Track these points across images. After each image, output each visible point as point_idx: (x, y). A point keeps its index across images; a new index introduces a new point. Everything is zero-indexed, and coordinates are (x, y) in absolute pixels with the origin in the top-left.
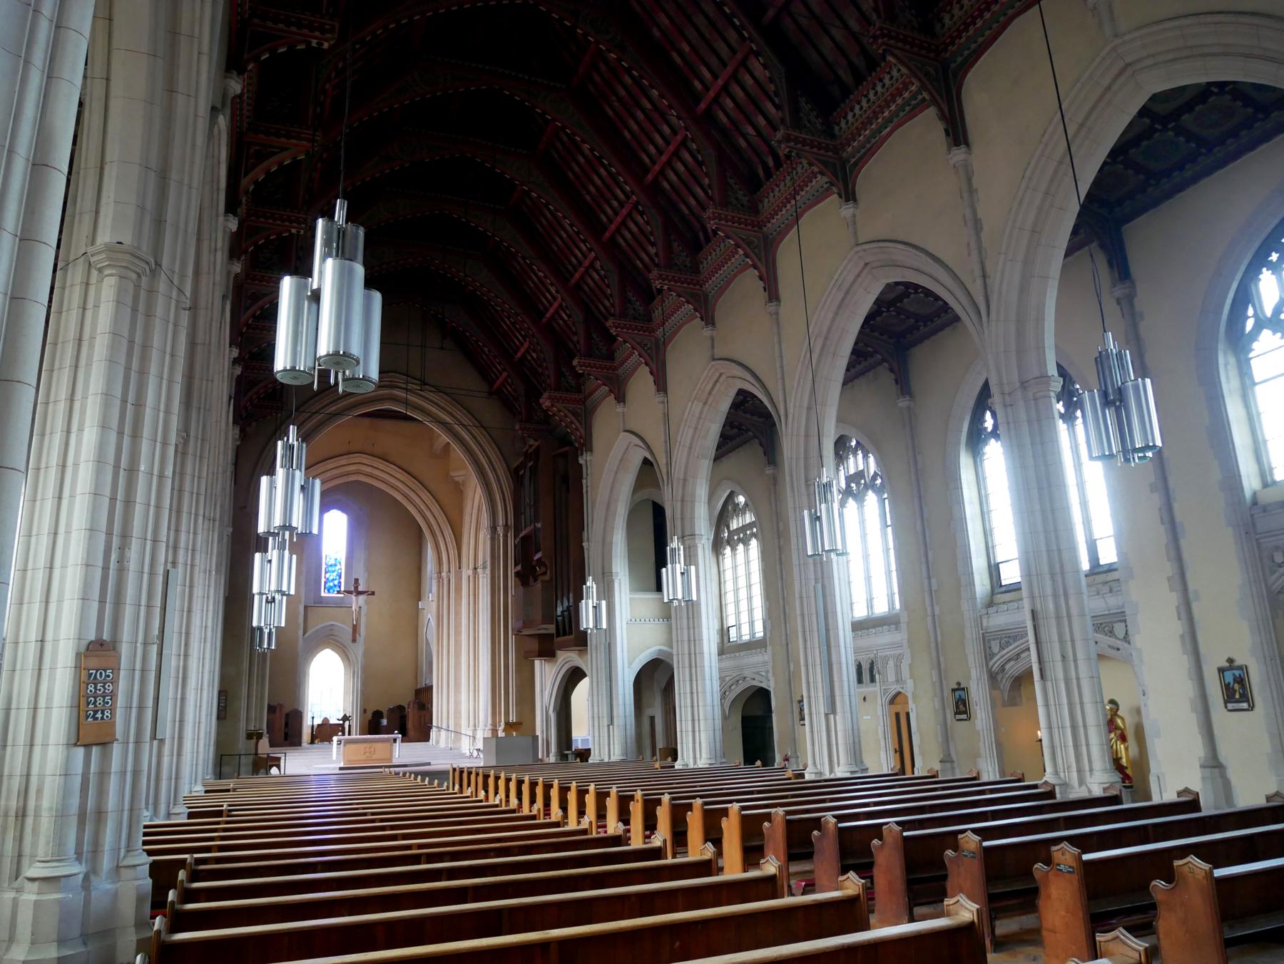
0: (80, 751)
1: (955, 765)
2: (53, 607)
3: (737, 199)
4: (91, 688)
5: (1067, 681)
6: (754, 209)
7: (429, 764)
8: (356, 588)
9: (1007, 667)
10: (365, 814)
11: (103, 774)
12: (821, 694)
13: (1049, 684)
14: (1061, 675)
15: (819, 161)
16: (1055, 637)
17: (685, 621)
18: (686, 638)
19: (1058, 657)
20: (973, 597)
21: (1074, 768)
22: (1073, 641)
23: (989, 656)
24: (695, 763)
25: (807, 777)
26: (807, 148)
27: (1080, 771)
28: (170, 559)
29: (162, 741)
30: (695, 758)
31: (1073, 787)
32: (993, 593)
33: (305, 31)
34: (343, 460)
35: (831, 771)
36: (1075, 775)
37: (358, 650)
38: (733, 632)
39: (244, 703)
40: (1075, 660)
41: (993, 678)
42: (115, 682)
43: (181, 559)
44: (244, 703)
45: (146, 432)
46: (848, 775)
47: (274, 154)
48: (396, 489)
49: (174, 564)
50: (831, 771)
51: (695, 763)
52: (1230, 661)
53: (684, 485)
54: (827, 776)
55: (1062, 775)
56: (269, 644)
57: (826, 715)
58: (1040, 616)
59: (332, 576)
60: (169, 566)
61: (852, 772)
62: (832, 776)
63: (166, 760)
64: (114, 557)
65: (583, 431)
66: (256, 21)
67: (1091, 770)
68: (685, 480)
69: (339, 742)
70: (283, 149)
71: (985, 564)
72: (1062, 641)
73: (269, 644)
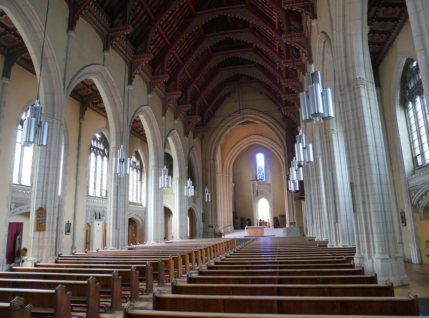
0: (38, 233)
1: (404, 245)
2: (341, 175)
3: (295, 28)
4: (39, 218)
5: (365, 213)
6: (302, 29)
7: (275, 236)
8: (257, 178)
9: (420, 202)
10: (323, 251)
11: (43, 238)
12: (332, 215)
13: (358, 214)
14: (362, 210)
15: (301, 7)
16: (360, 194)
17: (316, 186)
18: (316, 193)
19: (361, 203)
20: (404, 172)
21: (367, 251)
22: (368, 195)
23: (411, 198)
24: (322, 239)
25: (329, 247)
26: (294, 4)
27: (369, 253)
28: (119, 182)
29: (119, 229)
30: (322, 237)
31: (366, 260)
32: (414, 170)
33: (122, 31)
34: (249, 138)
35: (337, 244)
36: (367, 254)
37: (271, 198)
38: (419, 159)
39: (210, 217)
40: (369, 204)
41: (415, 208)
42: (45, 217)
43: (121, 182)
44: (210, 217)
45: (52, 157)
46: (342, 247)
47: (140, 64)
48: (267, 145)
49: (120, 183)
50: (337, 244)
51: (322, 239)
52: (69, 222)
53: (312, 136)
54: (335, 247)
55: (362, 254)
56: (208, 199)
57: (335, 223)
58: (354, 185)
59: (261, 174)
60: (119, 184)
61: (343, 246)
62: (337, 247)
63: (120, 234)
64: (45, 188)
65: (297, 120)
66: (110, 33)
67: (374, 253)
68: (312, 134)
69: (247, 229)
70: (142, 62)
71: (411, 157)
72: (363, 196)
73: (208, 199)
